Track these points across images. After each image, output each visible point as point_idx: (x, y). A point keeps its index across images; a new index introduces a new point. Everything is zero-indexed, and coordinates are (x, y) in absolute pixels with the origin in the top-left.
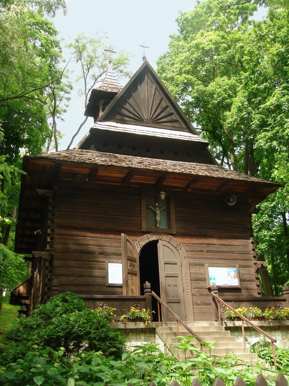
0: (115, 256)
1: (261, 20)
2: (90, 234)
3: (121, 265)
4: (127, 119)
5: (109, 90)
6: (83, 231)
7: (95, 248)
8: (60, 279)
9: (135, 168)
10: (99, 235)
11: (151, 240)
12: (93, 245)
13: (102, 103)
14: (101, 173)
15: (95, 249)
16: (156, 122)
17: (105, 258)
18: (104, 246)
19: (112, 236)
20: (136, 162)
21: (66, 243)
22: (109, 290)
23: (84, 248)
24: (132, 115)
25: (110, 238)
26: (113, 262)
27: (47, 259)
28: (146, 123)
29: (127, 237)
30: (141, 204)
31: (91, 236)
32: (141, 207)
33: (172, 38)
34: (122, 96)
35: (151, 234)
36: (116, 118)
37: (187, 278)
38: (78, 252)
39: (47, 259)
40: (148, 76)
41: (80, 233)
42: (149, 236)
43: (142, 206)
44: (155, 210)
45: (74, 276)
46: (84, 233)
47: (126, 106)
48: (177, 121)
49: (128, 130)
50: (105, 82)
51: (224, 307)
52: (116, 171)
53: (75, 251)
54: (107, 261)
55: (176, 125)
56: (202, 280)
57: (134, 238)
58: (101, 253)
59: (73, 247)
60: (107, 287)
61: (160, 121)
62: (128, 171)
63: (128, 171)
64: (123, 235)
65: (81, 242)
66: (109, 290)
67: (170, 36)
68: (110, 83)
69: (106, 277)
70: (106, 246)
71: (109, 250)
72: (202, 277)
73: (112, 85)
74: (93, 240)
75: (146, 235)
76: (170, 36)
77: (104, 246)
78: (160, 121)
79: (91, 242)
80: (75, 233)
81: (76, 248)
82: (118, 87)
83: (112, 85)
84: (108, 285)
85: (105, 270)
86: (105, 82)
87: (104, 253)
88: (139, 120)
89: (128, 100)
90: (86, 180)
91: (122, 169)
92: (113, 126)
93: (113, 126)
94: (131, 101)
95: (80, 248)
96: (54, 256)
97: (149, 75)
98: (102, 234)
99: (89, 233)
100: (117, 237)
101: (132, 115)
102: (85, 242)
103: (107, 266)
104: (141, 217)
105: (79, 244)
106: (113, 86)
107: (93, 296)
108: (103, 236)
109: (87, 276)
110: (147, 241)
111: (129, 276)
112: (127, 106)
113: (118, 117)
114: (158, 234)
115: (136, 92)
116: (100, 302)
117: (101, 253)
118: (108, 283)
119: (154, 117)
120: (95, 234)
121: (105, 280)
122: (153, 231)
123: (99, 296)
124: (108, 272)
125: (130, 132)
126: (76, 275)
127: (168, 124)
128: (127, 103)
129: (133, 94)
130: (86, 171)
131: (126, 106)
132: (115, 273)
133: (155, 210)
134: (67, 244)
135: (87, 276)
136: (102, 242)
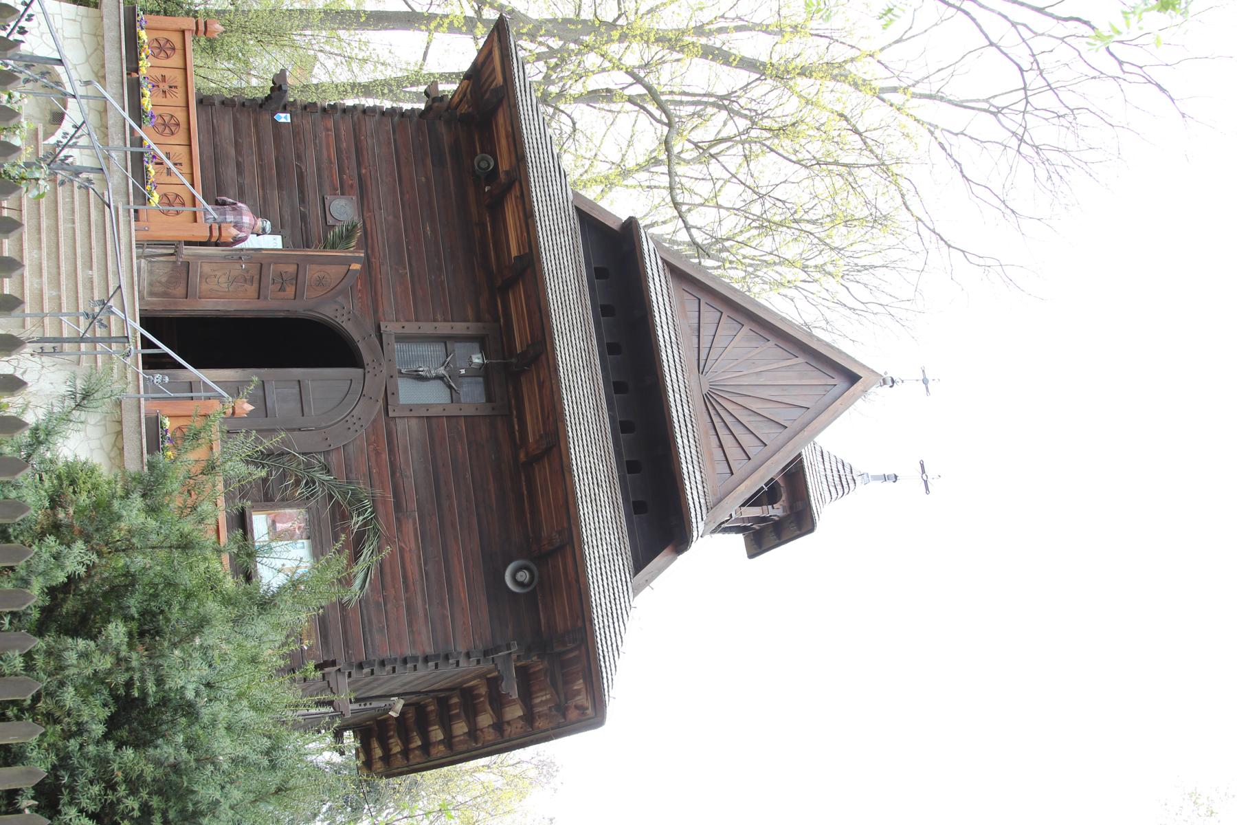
110: (356, 336)
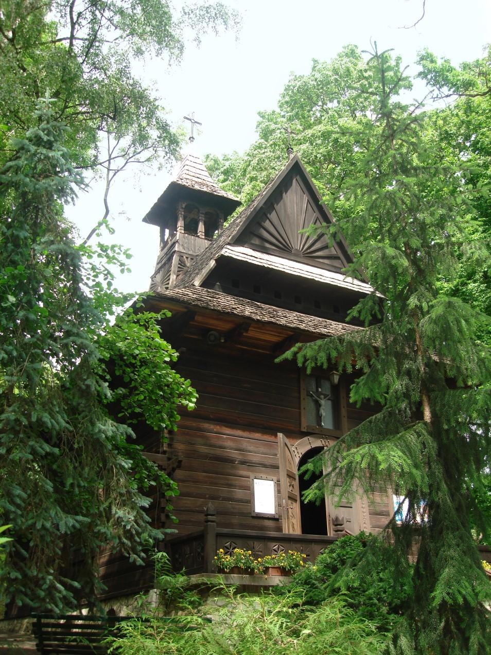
0: (270, 468)
1: (103, 46)
2: (227, 429)
3: (272, 483)
4: (268, 245)
5: (197, 187)
6: (217, 424)
7: (234, 453)
8: (185, 502)
9: (304, 330)
10: (239, 433)
11: (313, 446)
12: (231, 449)
13: (184, 206)
14: (252, 333)
15: (235, 454)
16: (308, 257)
17: (249, 470)
18: (247, 451)
19: (258, 435)
20: (291, 318)
21: (193, 442)
22: (256, 522)
23: (218, 452)
24: (274, 241)
25: (255, 438)
26: (261, 479)
27: (163, 467)
28: (296, 255)
29: (287, 441)
30: (299, 387)
31: (228, 432)
32: (299, 393)
33: (261, 117)
34: (261, 208)
35: (314, 437)
36: (253, 242)
37: (364, 510)
38: (211, 458)
39: (163, 467)
40: (296, 180)
41: (212, 427)
42: (311, 439)
43: (302, 391)
44: (318, 399)
45: (205, 498)
46: (218, 427)
47: (265, 224)
48: (338, 258)
49: (275, 264)
50: (187, 172)
51: (277, 550)
52: (272, 331)
53: (206, 456)
54: (252, 475)
55: (337, 263)
56: (383, 515)
57: (292, 441)
58: (243, 463)
59: (203, 449)
60: (253, 517)
61: (314, 255)
62: (292, 333)
63: (292, 333)
64: (280, 435)
65: (214, 441)
66: (256, 522)
67: (259, 113)
68: (194, 174)
69: (250, 501)
70: (250, 452)
71: (255, 458)
72: (384, 509)
73: (198, 178)
74: (231, 440)
75: (306, 438)
76: (259, 113)
77: (247, 451)
78: (314, 255)
79: (229, 444)
80: (206, 425)
81: (206, 451)
82: (208, 183)
83: (198, 178)
84: (255, 515)
85: (250, 489)
86: (187, 172)
87: (247, 463)
88: (284, 250)
89: (268, 215)
90: (220, 340)
91: (285, 330)
92: (251, 256)
93: (251, 256)
94: (273, 216)
95: (212, 452)
96: (182, 464)
97: (298, 178)
98: (244, 430)
99: (224, 428)
100: (272, 439)
101: (274, 241)
102: (220, 443)
103: (253, 483)
104: (300, 409)
105: (211, 446)
106: (199, 180)
107: (266, 534)
108: (246, 434)
109: (225, 499)
111: (290, 501)
112: (267, 224)
113: (257, 241)
114: (323, 438)
115: (281, 203)
116: (274, 544)
117: (243, 463)
118: (254, 511)
119: (305, 248)
120: (235, 431)
121: (251, 506)
122: (317, 431)
123: (274, 534)
124: (254, 495)
125: (277, 268)
126: (207, 496)
127: (326, 261)
128: (268, 220)
129: (275, 206)
130: (226, 327)
131: (265, 224)
132: (265, 497)
133: (318, 399)
134: (193, 444)
135: (225, 499)
136: (245, 444)
